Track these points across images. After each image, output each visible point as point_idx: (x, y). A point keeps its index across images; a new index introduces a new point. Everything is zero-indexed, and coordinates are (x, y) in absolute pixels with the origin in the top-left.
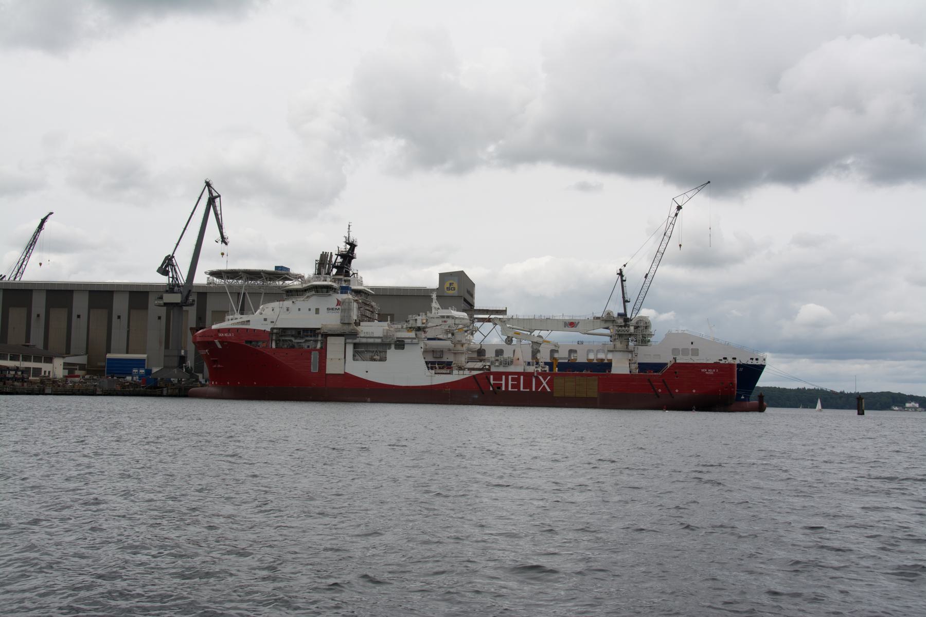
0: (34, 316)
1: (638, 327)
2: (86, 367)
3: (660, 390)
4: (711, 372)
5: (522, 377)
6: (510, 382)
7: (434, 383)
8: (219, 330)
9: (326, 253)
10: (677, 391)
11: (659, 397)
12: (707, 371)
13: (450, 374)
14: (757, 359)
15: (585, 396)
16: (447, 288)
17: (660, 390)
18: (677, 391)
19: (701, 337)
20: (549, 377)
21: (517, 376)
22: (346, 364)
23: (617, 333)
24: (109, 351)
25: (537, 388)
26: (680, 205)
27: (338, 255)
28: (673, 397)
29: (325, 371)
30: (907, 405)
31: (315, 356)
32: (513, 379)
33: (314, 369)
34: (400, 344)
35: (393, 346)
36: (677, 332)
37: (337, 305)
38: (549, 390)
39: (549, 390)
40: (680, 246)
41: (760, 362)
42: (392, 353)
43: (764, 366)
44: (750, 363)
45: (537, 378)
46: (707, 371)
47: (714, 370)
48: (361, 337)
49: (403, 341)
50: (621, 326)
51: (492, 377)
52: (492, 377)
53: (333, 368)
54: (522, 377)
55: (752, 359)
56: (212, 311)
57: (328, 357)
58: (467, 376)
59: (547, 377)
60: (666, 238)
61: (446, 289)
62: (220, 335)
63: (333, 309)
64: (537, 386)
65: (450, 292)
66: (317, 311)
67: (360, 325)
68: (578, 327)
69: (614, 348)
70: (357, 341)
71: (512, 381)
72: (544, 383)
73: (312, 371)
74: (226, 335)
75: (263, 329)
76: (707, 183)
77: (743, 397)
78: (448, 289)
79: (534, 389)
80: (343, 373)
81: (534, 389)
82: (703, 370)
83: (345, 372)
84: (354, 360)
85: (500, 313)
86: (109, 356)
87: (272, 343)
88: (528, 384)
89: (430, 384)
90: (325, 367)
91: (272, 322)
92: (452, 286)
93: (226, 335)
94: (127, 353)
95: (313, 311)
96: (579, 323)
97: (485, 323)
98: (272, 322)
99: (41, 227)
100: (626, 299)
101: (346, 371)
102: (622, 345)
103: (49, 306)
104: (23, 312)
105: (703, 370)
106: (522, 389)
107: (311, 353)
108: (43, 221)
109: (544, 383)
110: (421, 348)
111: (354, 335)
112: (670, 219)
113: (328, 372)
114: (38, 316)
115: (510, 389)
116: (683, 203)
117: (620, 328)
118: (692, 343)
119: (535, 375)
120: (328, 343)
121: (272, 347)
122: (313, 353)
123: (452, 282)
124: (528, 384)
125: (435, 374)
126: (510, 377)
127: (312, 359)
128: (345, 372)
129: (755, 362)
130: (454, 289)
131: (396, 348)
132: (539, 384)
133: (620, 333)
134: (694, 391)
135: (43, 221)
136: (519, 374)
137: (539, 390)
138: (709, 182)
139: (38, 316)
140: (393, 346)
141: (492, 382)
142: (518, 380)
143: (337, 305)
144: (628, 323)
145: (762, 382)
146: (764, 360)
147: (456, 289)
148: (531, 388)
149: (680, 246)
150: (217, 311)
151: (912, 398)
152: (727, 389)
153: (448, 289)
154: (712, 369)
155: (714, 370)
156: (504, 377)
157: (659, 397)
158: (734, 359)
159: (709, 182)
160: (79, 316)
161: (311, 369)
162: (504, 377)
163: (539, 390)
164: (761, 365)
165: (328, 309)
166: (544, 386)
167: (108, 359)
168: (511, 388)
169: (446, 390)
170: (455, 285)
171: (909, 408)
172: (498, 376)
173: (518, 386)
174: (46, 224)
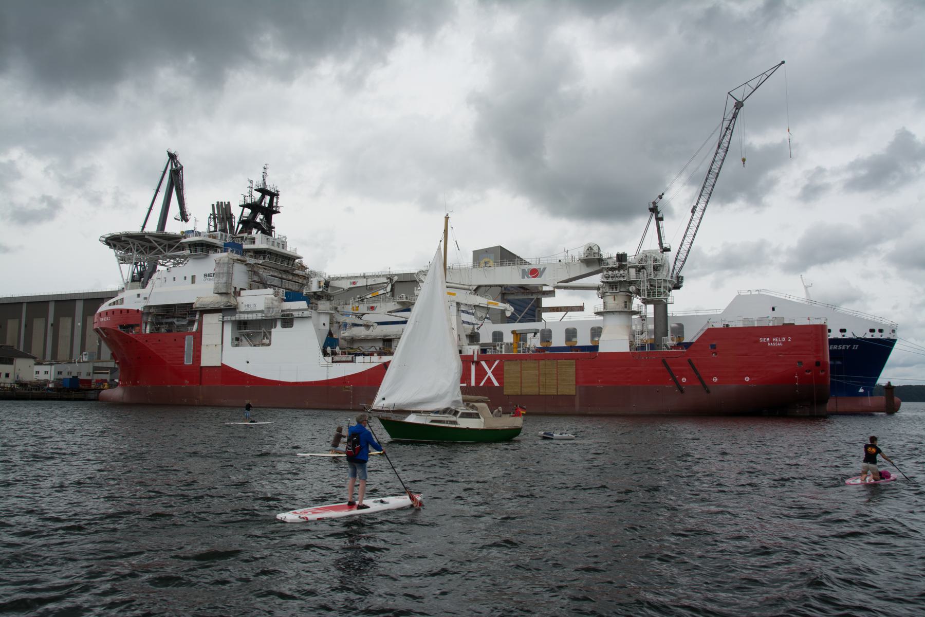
1: (643, 268)
3: (684, 380)
4: (777, 342)
7: (330, 378)
9: (222, 203)
10: (715, 379)
11: (682, 391)
13: (352, 361)
14: (881, 331)
15: (554, 392)
17: (684, 380)
18: (715, 379)
19: (787, 298)
20: (496, 363)
22: (224, 352)
23: (605, 280)
25: (478, 380)
26: (741, 100)
27: (244, 206)
28: (708, 392)
29: (200, 363)
31: (189, 341)
33: (188, 361)
34: (288, 321)
35: (279, 324)
36: (749, 293)
38: (496, 384)
39: (496, 384)
40: (744, 160)
41: (885, 336)
42: (278, 332)
43: (895, 341)
44: (869, 336)
46: (771, 341)
48: (241, 312)
49: (292, 315)
50: (613, 269)
53: (209, 359)
55: (872, 331)
57: (203, 344)
58: (377, 364)
60: (721, 152)
64: (479, 378)
67: (239, 295)
69: (604, 308)
70: (237, 317)
72: (490, 373)
73: (185, 363)
75: (136, 309)
76: (780, 64)
77: (861, 390)
79: (473, 384)
80: (220, 365)
81: (473, 384)
82: (762, 340)
83: (222, 364)
85: (547, 294)
87: (146, 328)
89: (325, 379)
90: (199, 360)
91: (145, 298)
95: (189, 279)
96: (545, 269)
97: (569, 313)
100: (664, 246)
101: (223, 362)
102: (616, 302)
105: (762, 340)
107: (184, 338)
109: (490, 373)
111: (231, 309)
112: (726, 124)
113: (202, 365)
116: (744, 98)
117: (610, 273)
118: (773, 309)
119: (475, 359)
120: (204, 322)
121: (145, 332)
122: (187, 337)
123: (487, 260)
125: (333, 362)
127: (186, 346)
128: (222, 364)
129: (877, 335)
131: (284, 326)
132: (481, 373)
133: (610, 280)
134: (747, 379)
137: (482, 384)
138: (783, 62)
140: (279, 324)
144: (624, 263)
145: (889, 376)
146: (893, 331)
149: (744, 160)
152: (810, 373)
154: (780, 336)
157: (682, 391)
158: (843, 331)
159: (783, 62)
161: (183, 360)
163: (482, 384)
164: (889, 339)
165: (205, 275)
169: (347, 387)
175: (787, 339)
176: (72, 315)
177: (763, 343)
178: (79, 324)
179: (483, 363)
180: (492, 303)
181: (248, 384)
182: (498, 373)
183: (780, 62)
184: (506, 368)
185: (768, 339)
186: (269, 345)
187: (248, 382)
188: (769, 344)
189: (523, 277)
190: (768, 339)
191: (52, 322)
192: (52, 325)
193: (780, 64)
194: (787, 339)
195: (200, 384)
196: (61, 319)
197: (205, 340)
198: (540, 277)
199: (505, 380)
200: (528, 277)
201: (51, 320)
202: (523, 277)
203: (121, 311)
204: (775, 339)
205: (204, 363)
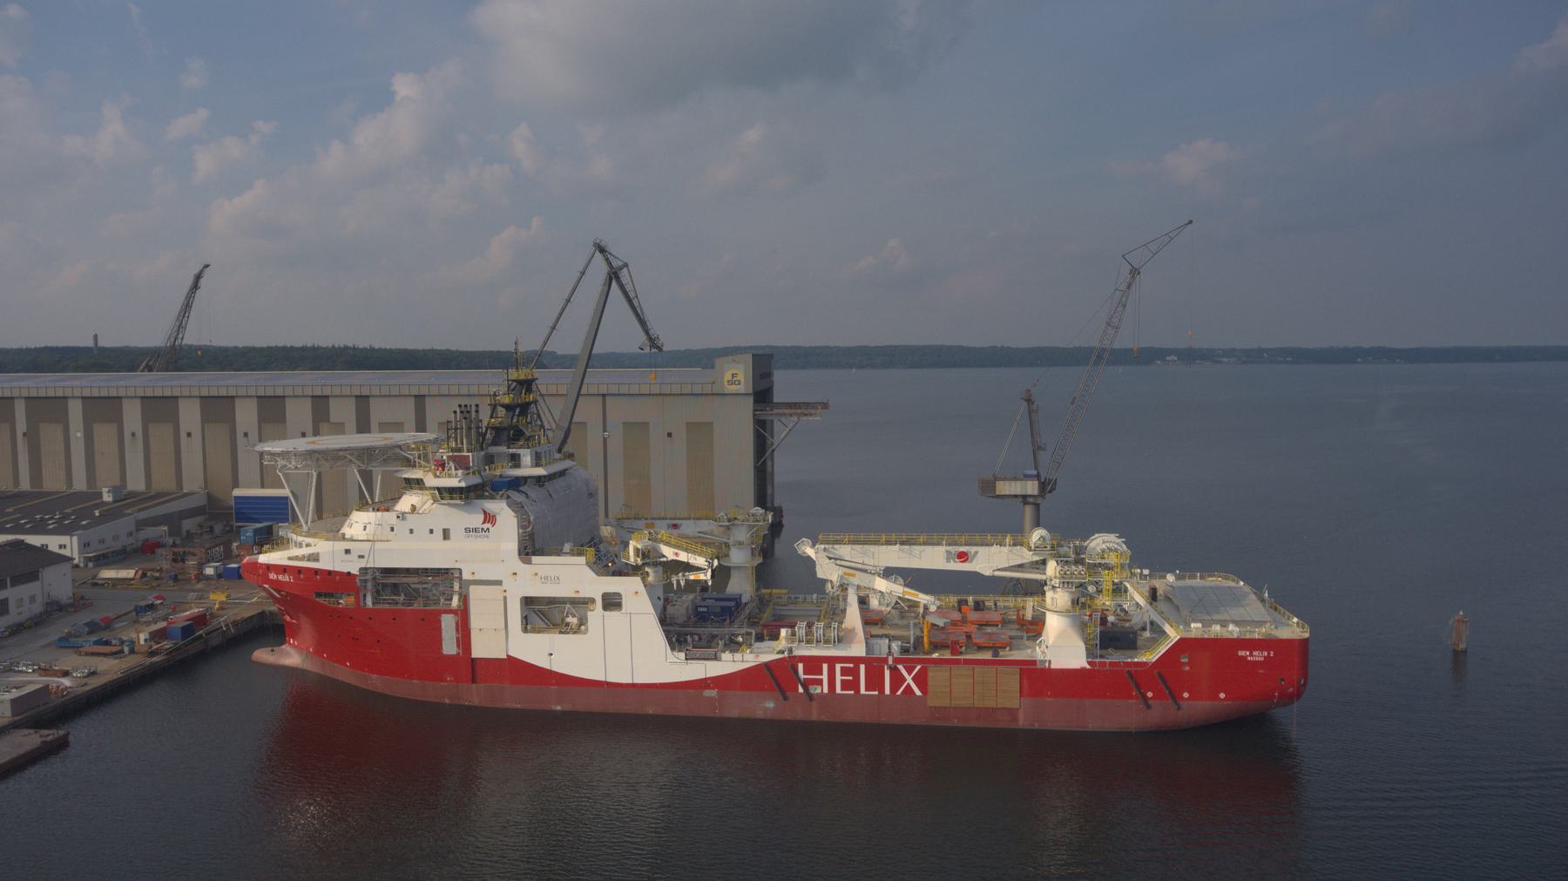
0: (240, 435)
2: (207, 508)
4: (1258, 656)
5: (862, 667)
6: (839, 678)
8: (269, 567)
12: (1251, 655)
16: (728, 381)
18: (1186, 695)
21: (851, 678)
24: (236, 485)
25: (894, 689)
30: (1168, 358)
31: (448, 623)
32: (844, 672)
33: (449, 647)
37: (484, 523)
39: (918, 692)
45: (894, 670)
46: (1251, 655)
47: (1266, 654)
51: (801, 666)
52: (801, 666)
53: (483, 648)
54: (862, 667)
56: (379, 424)
59: (914, 668)
61: (726, 383)
62: (272, 576)
63: (476, 530)
65: (734, 388)
66: (446, 534)
68: (974, 562)
71: (842, 675)
74: (280, 577)
75: (345, 571)
76: (1187, 224)
78: (731, 383)
79: (887, 691)
80: (505, 657)
81: (887, 691)
82: (1241, 653)
83: (508, 655)
84: (525, 630)
86: (237, 492)
88: (875, 681)
91: (361, 557)
92: (735, 379)
93: (280, 577)
94: (263, 487)
95: (439, 533)
98: (361, 557)
99: (195, 286)
103: (147, 420)
104: (112, 429)
105: (1241, 653)
106: (863, 691)
108: (198, 277)
110: (659, 598)
113: (474, 656)
114: (133, 434)
115: (838, 690)
124: (875, 681)
126: (838, 667)
128: (508, 655)
130: (739, 384)
132: (897, 680)
135: (198, 277)
136: (856, 661)
137: (899, 693)
138: (1191, 222)
139: (133, 434)
141: (802, 676)
142: (855, 672)
143: (484, 523)
147: (742, 381)
148: (882, 690)
150: (390, 423)
151: (1171, 352)
153: (731, 383)
155: (1266, 654)
156: (825, 667)
160: (189, 435)
162: (825, 667)
165: (467, 530)
166: (909, 685)
167: (235, 497)
168: (842, 690)
170: (741, 377)
171: (1169, 361)
172: (813, 664)
173: (854, 685)
174: (203, 282)
175: (1269, 654)
176: (63, 419)
177: (1242, 656)
178: (79, 435)
179: (900, 667)
180: (910, 593)
181: (554, 685)
182: (921, 680)
183: (1187, 222)
184: (930, 674)
185: (1248, 653)
186: (577, 631)
187: (554, 681)
188: (1249, 658)
189: (948, 561)
190: (1248, 653)
191: (25, 430)
192: (24, 434)
193: (1187, 224)
194: (1269, 654)
195: (474, 682)
196: (150, 425)
197: (475, 623)
198: (971, 562)
199: (930, 689)
200: (955, 562)
201: (21, 426)
202: (948, 561)
203: (317, 571)
204: (1255, 653)
205: (478, 651)
